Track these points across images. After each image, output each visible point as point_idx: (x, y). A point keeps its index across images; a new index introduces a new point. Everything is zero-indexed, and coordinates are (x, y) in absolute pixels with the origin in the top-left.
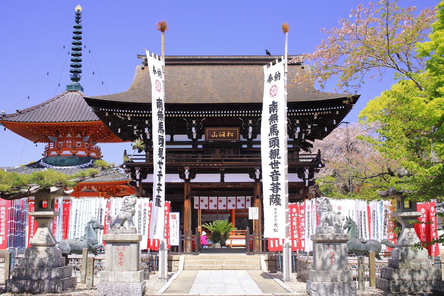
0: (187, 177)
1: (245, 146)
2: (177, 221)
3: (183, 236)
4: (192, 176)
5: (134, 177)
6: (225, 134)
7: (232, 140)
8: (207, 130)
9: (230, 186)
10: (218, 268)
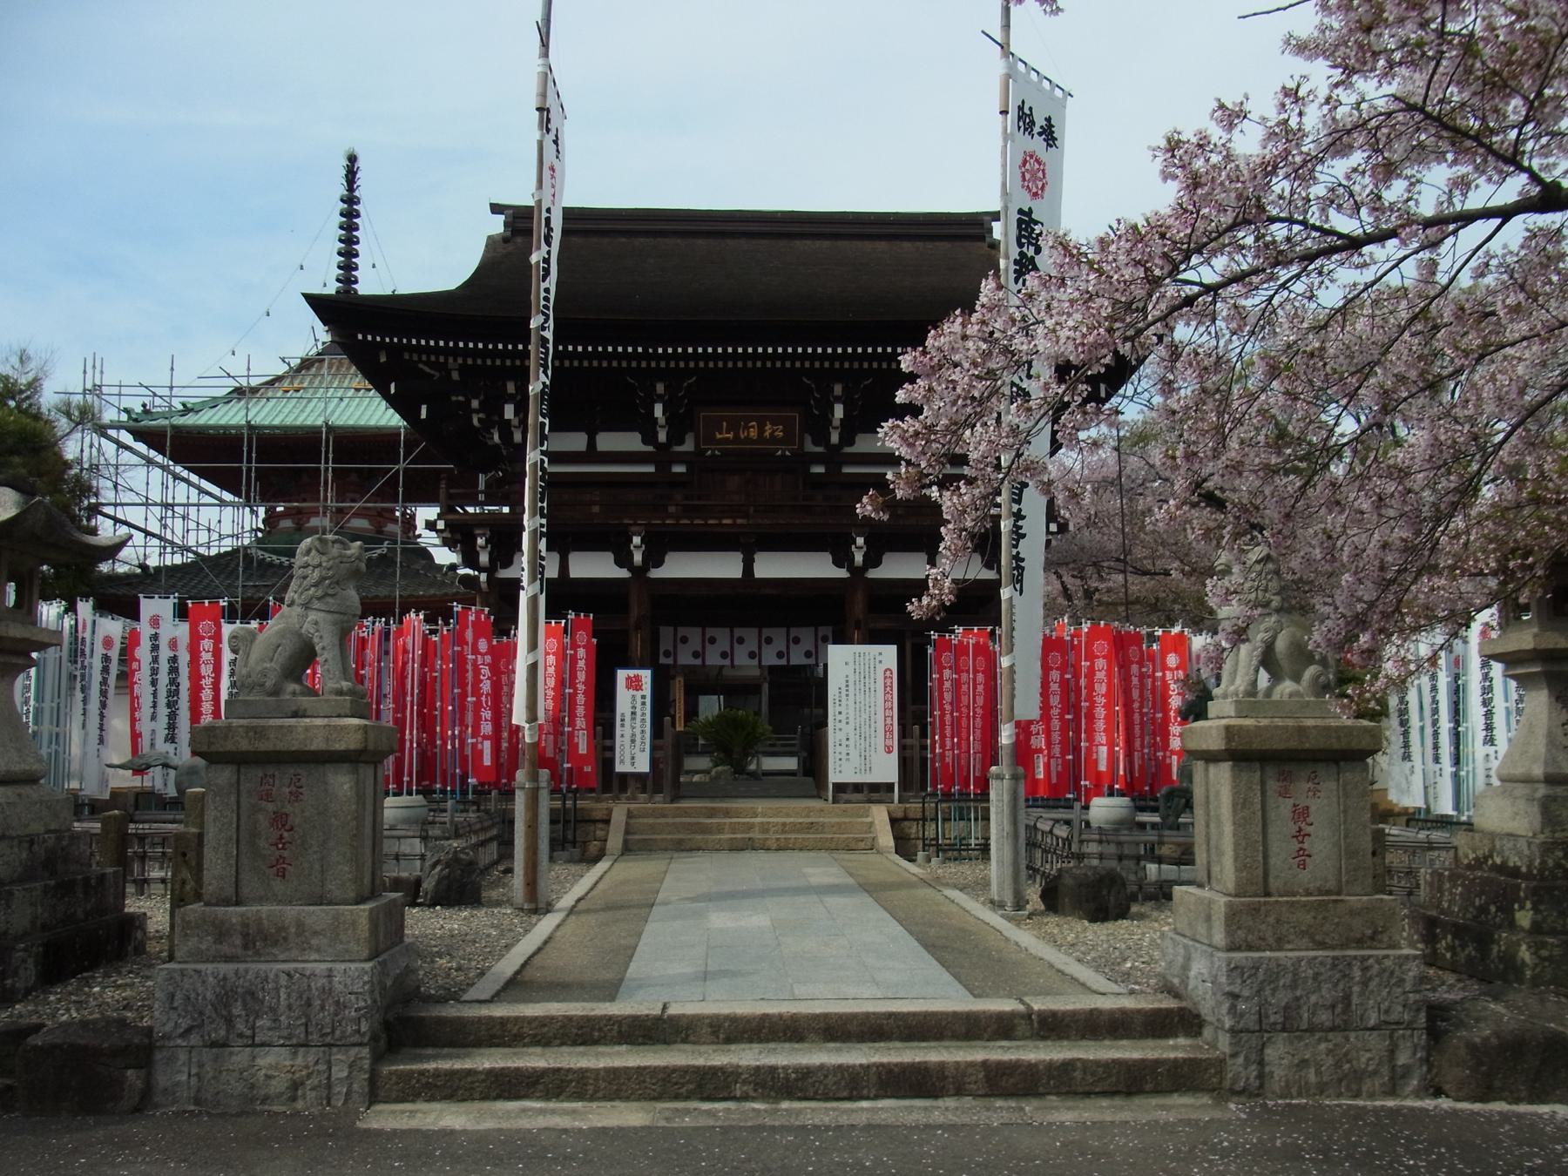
0: (638, 558)
1: (819, 469)
2: (643, 697)
3: (658, 742)
4: (655, 557)
6: (761, 430)
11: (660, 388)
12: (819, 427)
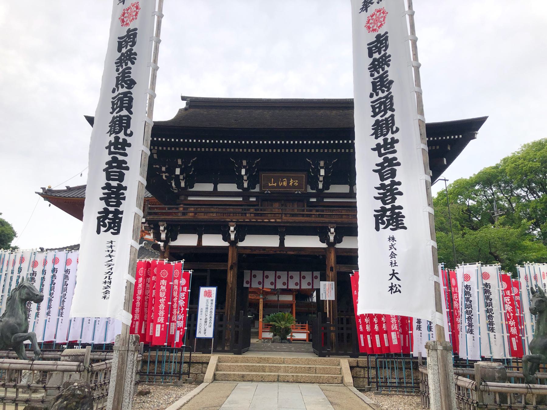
0: (232, 237)
2: (212, 300)
3: (221, 323)
5: (157, 236)
6: (289, 182)
7: (296, 191)
9: (292, 253)
10: (271, 378)
11: (244, 163)
12: (313, 181)
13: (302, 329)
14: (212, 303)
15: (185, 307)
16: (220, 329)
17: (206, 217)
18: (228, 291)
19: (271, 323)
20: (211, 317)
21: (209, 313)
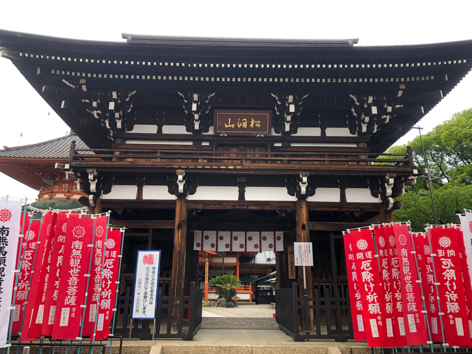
0: (181, 188)
2: (154, 268)
3: (165, 298)
5: (85, 187)
8: (218, 114)
9: (254, 208)
11: (196, 97)
12: (278, 123)
13: (244, 289)
14: (154, 272)
15: (113, 280)
16: (165, 306)
17: (148, 163)
18: (175, 256)
19: (217, 285)
20: (152, 291)
21: (149, 285)
